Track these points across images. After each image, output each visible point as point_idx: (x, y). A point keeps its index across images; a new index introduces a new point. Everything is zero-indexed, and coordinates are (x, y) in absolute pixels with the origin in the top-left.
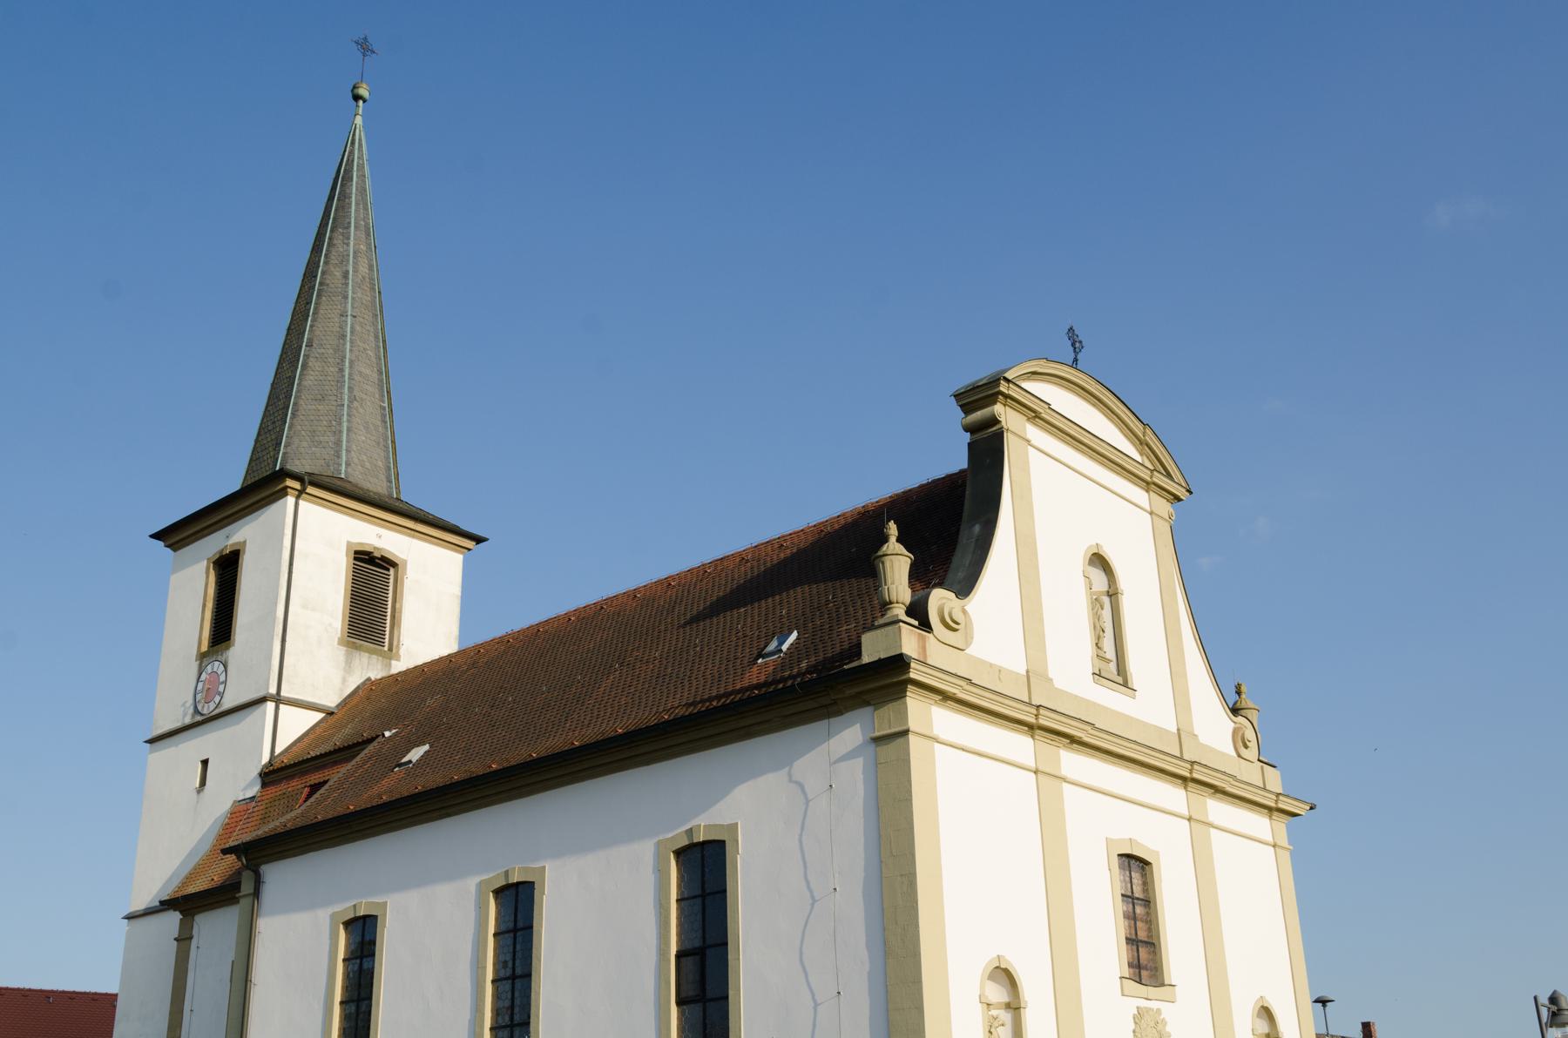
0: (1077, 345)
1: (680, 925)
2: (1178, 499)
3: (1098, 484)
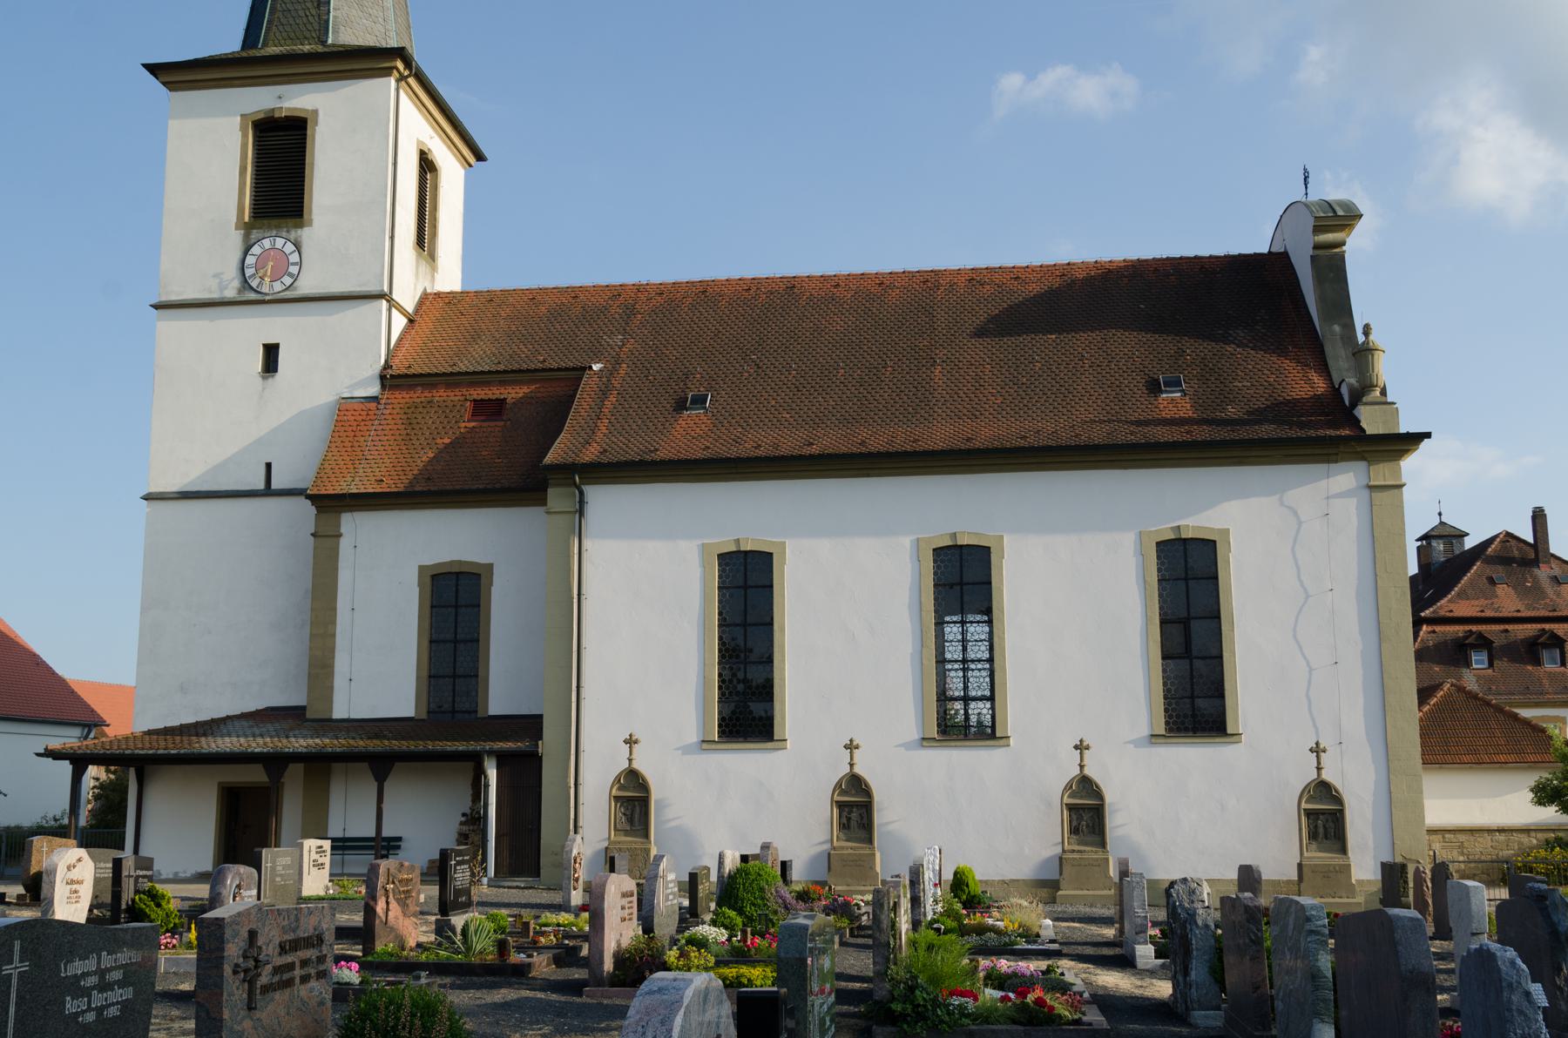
2: (470, 166)
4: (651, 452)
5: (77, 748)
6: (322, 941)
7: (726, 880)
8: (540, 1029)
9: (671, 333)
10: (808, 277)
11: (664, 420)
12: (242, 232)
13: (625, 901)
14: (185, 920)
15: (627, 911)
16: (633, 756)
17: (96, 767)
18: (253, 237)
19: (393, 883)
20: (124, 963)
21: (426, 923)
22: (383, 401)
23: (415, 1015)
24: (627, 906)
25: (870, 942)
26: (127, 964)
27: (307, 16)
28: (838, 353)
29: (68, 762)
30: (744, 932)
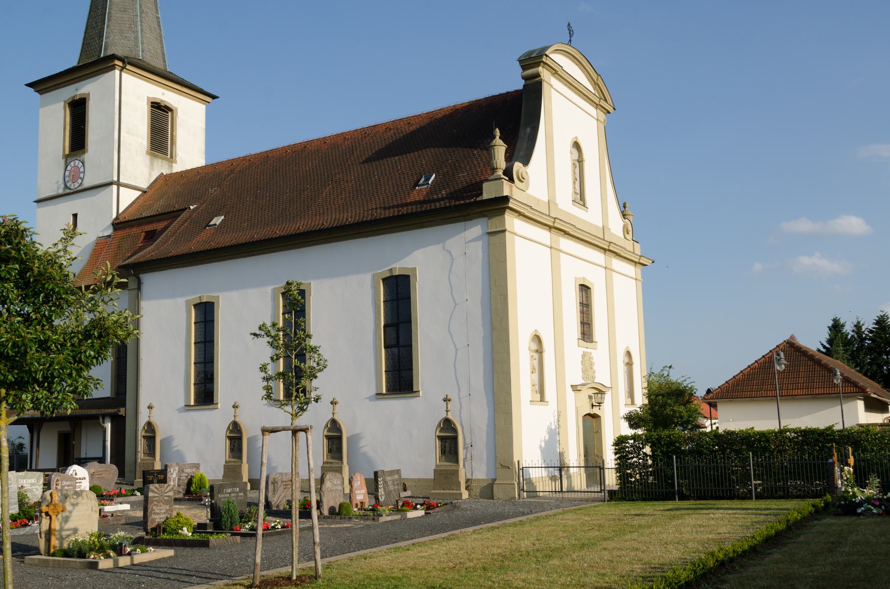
0: (571, 33)
1: (385, 310)
2: (609, 112)
3: (572, 102)
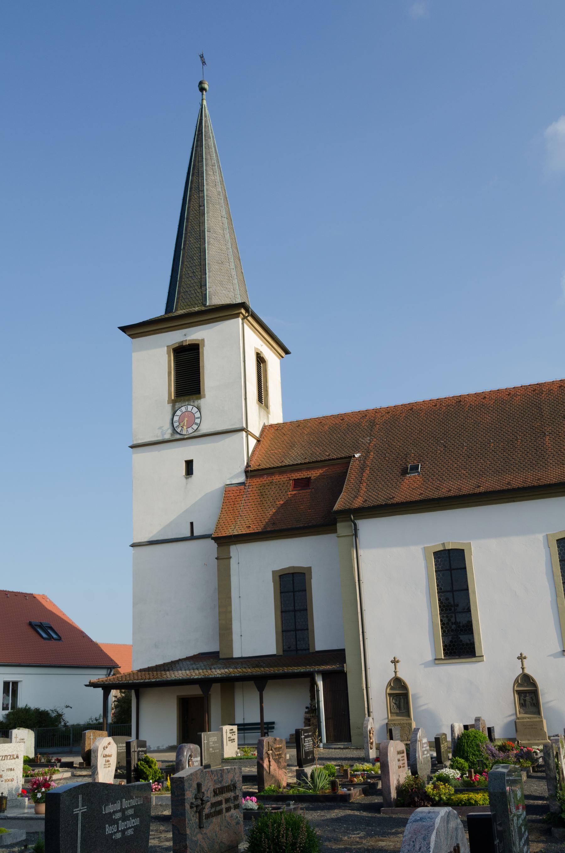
2: (282, 357)
4: (391, 499)
5: (105, 681)
6: (236, 788)
7: (456, 741)
8: (358, 834)
9: (396, 433)
10: (468, 395)
11: (396, 481)
12: (171, 404)
13: (399, 756)
14: (164, 775)
15: (401, 762)
16: (397, 670)
17: (115, 690)
18: (177, 406)
19: (272, 750)
20: (134, 805)
21: (291, 771)
22: (247, 485)
23: (288, 829)
24: (401, 759)
25: (543, 774)
26: (135, 805)
27: (195, 293)
28: (489, 434)
29: (101, 689)
30: (470, 772)
